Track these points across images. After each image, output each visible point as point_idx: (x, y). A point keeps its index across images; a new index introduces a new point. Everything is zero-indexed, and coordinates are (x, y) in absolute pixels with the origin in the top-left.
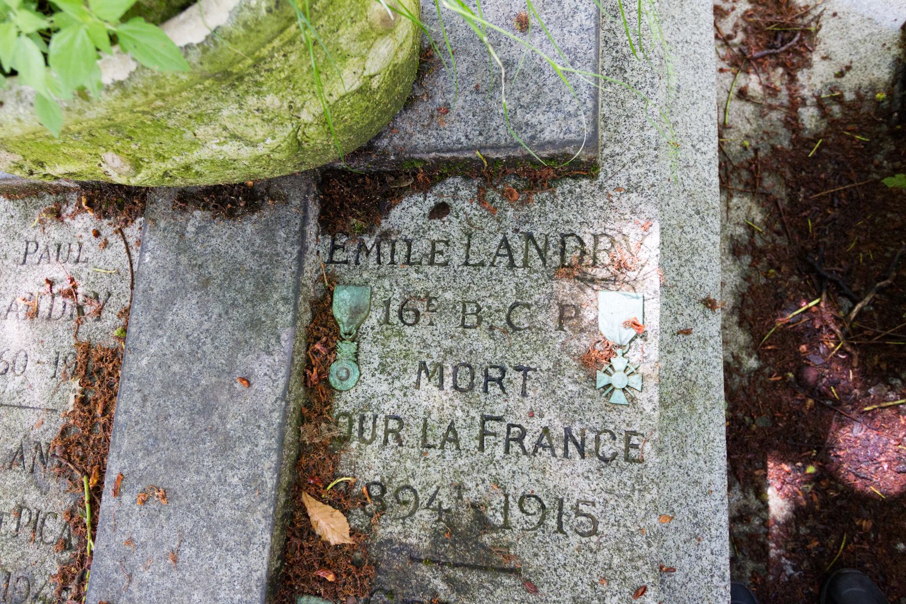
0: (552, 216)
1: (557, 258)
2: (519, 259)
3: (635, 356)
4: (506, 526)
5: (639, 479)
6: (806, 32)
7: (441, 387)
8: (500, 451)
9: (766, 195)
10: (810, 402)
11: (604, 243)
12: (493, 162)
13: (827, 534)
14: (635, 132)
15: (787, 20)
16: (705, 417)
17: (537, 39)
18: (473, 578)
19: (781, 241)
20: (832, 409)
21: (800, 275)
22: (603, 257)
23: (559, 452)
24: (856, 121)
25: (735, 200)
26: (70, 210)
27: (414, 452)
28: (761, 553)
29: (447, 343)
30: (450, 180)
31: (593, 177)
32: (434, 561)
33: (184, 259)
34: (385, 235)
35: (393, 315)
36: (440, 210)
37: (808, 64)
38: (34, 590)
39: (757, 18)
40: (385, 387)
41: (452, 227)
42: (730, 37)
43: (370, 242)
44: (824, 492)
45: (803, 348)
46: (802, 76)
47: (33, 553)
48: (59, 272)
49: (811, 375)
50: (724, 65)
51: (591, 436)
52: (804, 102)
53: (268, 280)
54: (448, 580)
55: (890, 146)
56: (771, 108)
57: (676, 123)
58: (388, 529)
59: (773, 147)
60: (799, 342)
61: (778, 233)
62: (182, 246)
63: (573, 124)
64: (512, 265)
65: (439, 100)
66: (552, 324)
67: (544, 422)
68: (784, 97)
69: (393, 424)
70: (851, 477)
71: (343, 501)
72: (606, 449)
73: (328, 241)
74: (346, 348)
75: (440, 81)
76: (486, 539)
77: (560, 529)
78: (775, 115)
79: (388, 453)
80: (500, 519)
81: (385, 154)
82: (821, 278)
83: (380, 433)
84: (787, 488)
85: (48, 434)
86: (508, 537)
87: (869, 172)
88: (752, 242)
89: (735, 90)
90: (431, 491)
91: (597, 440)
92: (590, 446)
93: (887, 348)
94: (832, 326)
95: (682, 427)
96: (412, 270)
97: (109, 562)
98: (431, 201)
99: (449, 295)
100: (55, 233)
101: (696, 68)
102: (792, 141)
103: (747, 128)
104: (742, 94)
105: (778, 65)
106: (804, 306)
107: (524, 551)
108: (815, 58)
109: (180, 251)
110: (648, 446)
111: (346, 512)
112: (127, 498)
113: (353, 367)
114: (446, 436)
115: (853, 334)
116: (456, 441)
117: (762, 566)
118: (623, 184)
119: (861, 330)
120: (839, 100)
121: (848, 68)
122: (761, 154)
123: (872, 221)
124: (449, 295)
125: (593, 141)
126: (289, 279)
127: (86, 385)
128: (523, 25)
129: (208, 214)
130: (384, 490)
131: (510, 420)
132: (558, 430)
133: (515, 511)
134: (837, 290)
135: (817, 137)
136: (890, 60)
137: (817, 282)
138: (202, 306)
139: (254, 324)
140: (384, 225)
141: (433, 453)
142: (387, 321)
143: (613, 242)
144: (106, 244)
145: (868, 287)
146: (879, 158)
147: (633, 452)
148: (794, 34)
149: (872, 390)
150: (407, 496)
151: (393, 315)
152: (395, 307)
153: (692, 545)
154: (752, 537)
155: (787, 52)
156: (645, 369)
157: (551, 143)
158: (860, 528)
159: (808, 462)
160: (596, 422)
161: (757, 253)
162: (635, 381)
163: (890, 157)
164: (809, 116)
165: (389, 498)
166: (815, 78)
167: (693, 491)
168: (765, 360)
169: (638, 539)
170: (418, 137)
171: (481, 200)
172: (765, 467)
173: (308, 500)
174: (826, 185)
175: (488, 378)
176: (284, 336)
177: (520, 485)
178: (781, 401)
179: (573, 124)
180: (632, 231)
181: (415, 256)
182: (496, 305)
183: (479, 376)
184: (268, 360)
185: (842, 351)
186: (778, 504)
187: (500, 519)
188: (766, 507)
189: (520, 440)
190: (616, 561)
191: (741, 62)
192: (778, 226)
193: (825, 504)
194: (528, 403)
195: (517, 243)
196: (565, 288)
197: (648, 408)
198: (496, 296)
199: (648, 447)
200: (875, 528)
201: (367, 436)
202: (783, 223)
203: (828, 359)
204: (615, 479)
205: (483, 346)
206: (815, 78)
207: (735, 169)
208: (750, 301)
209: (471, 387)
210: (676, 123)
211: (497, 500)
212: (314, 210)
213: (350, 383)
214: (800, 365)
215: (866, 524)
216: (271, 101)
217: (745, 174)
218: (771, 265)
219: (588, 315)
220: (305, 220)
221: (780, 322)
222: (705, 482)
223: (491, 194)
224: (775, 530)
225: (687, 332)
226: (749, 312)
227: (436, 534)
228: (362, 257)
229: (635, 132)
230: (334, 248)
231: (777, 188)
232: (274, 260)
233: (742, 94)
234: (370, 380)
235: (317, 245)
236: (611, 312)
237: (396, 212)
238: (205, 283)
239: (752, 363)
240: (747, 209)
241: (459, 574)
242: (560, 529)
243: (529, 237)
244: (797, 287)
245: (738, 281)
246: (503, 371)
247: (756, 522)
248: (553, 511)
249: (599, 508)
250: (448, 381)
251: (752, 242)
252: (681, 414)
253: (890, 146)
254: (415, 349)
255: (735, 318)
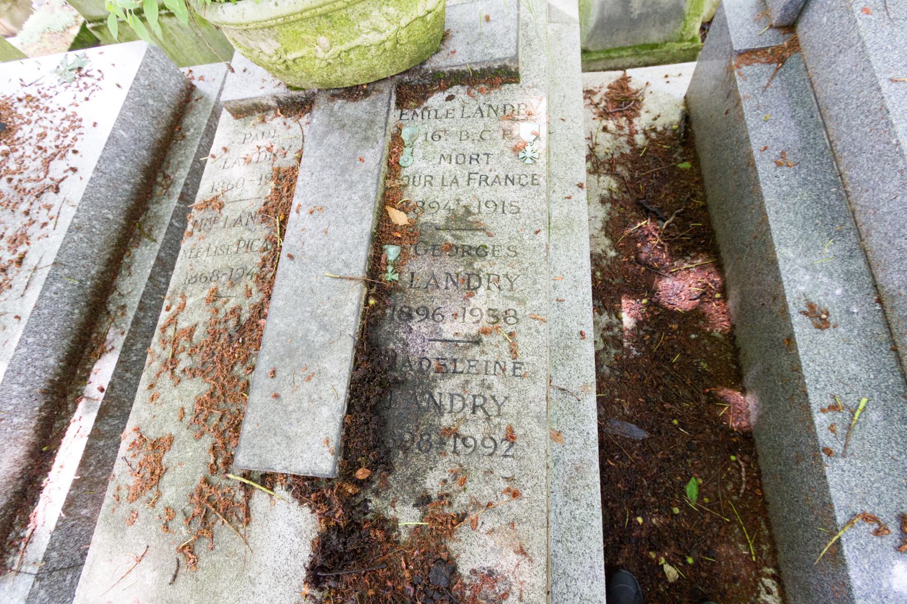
0: (500, 98)
1: (502, 113)
2: (485, 114)
3: (535, 147)
4: (479, 212)
5: (538, 191)
6: (637, 101)
7: (450, 163)
8: (477, 185)
9: (617, 175)
10: (643, 269)
11: (523, 107)
12: (474, 72)
13: (654, 333)
14: (536, 67)
15: (627, 95)
16: (579, 235)
17: (493, 24)
18: (464, 233)
19: (627, 196)
20: (654, 271)
21: (637, 211)
22: (522, 112)
23: (503, 184)
24: (663, 139)
25: (602, 178)
26: (270, 117)
27: (438, 188)
28: (619, 344)
29: (454, 147)
30: (455, 87)
31: (517, 82)
32: (447, 229)
33: (332, 119)
34: (426, 108)
35: (429, 138)
36: (450, 98)
37: (638, 115)
38: (246, 272)
39: (612, 95)
40: (425, 165)
41: (456, 103)
42: (598, 104)
43: (418, 111)
44: (652, 313)
45: (639, 245)
46: (635, 121)
47: (246, 257)
48: (264, 142)
49: (643, 256)
50: (595, 116)
51: (517, 177)
52: (637, 132)
53: (372, 121)
54: (453, 236)
55: (681, 150)
56: (620, 135)
57: (563, 111)
58: (425, 218)
59: (622, 153)
60: (637, 242)
61: (625, 192)
62: (332, 114)
63: (508, 52)
64: (482, 116)
65: (452, 49)
66: (500, 137)
67: (496, 173)
68: (627, 130)
69: (428, 178)
70: (666, 304)
71: (405, 208)
72: (523, 182)
73: (399, 112)
74: (407, 150)
75: (452, 42)
76: (470, 219)
77: (503, 212)
78: (622, 139)
79: (426, 189)
80: (476, 211)
81: (427, 70)
82: (647, 211)
83: (422, 182)
84: (633, 312)
85: (258, 205)
86: (480, 217)
87: (671, 162)
88: (611, 197)
89: (601, 128)
90: (445, 203)
91: (520, 178)
92: (516, 180)
93: (682, 241)
94: (654, 233)
95: (567, 239)
96: (438, 121)
97: (293, 239)
98: (446, 94)
99: (454, 129)
100: (261, 128)
101: (573, 88)
102: (631, 150)
103: (608, 145)
104: (605, 129)
105: (623, 116)
106: (639, 225)
107: (486, 221)
108: (642, 112)
109: (331, 116)
110: (541, 179)
111: (407, 213)
112: (302, 213)
113: (410, 157)
114: (453, 182)
115: (665, 236)
116: (457, 183)
117: (620, 351)
118: (531, 85)
119: (668, 234)
120: (654, 130)
121: (659, 116)
122: (615, 156)
123: (673, 184)
124: (454, 129)
125: (515, 59)
126: (383, 120)
127: (277, 184)
128: (487, 19)
129: (345, 101)
130: (424, 204)
131: (481, 173)
132: (502, 176)
133: (483, 207)
134: (657, 217)
135: (644, 147)
136: (679, 112)
137: (646, 213)
138: (341, 135)
139: (366, 139)
140: (425, 104)
141: (446, 188)
142: (426, 140)
143: (526, 106)
144: (289, 127)
145: (671, 215)
146: (675, 156)
147: (535, 182)
148: (631, 101)
149: (675, 263)
150: (435, 205)
151: (429, 138)
152: (430, 135)
153: (573, 291)
154: (614, 337)
155: (628, 110)
156: (540, 151)
157: (499, 59)
158: (671, 328)
159: (642, 298)
160: (519, 171)
161: (614, 202)
162: (536, 155)
163: (681, 155)
164: (640, 139)
165: (426, 206)
166: (642, 121)
167: (573, 266)
168: (619, 252)
169: (537, 213)
170: (441, 62)
171: (469, 93)
172: (620, 303)
173: (388, 208)
174: (649, 168)
175: (471, 158)
176: (380, 141)
177: (486, 197)
178: (628, 270)
179: (508, 52)
180: (535, 102)
181: (439, 115)
182: (475, 131)
183: (468, 158)
184: (373, 151)
185: (659, 244)
186: (628, 321)
187: (476, 211)
188: (622, 323)
189: (486, 181)
190: (528, 222)
191: (605, 114)
192: (624, 189)
193: (653, 317)
194: (489, 167)
195: (485, 108)
196: (506, 124)
197: (541, 165)
198: (476, 128)
199: (541, 179)
200: (679, 329)
201: (416, 184)
202: (627, 187)
203: (652, 248)
204: (527, 192)
205: (470, 147)
206: (642, 121)
207: (602, 163)
208: (611, 224)
209: (464, 162)
210: (563, 111)
211: (476, 204)
212: (394, 97)
213: (409, 163)
214: (637, 252)
215: (675, 326)
216: (391, 10)
217: (607, 166)
218: (621, 206)
219: (515, 133)
220: (390, 98)
221: (627, 232)
222: (579, 262)
223: (473, 91)
224: (626, 333)
225: (569, 198)
226: (610, 230)
227: (448, 218)
228: (415, 117)
229: (536, 67)
230: (402, 114)
231: (624, 172)
232: (376, 114)
233: (605, 129)
234: (418, 162)
235: (395, 114)
236: (524, 131)
237: (430, 100)
238: (343, 126)
239: (613, 254)
240: (608, 182)
241: (458, 232)
242: (503, 212)
243: (490, 106)
244: (634, 217)
245: (605, 215)
246: (478, 156)
247: (616, 330)
248: (501, 206)
249: (520, 203)
250: (454, 161)
251: (611, 197)
252: (567, 233)
253: (681, 150)
254: (439, 150)
255: (603, 233)
